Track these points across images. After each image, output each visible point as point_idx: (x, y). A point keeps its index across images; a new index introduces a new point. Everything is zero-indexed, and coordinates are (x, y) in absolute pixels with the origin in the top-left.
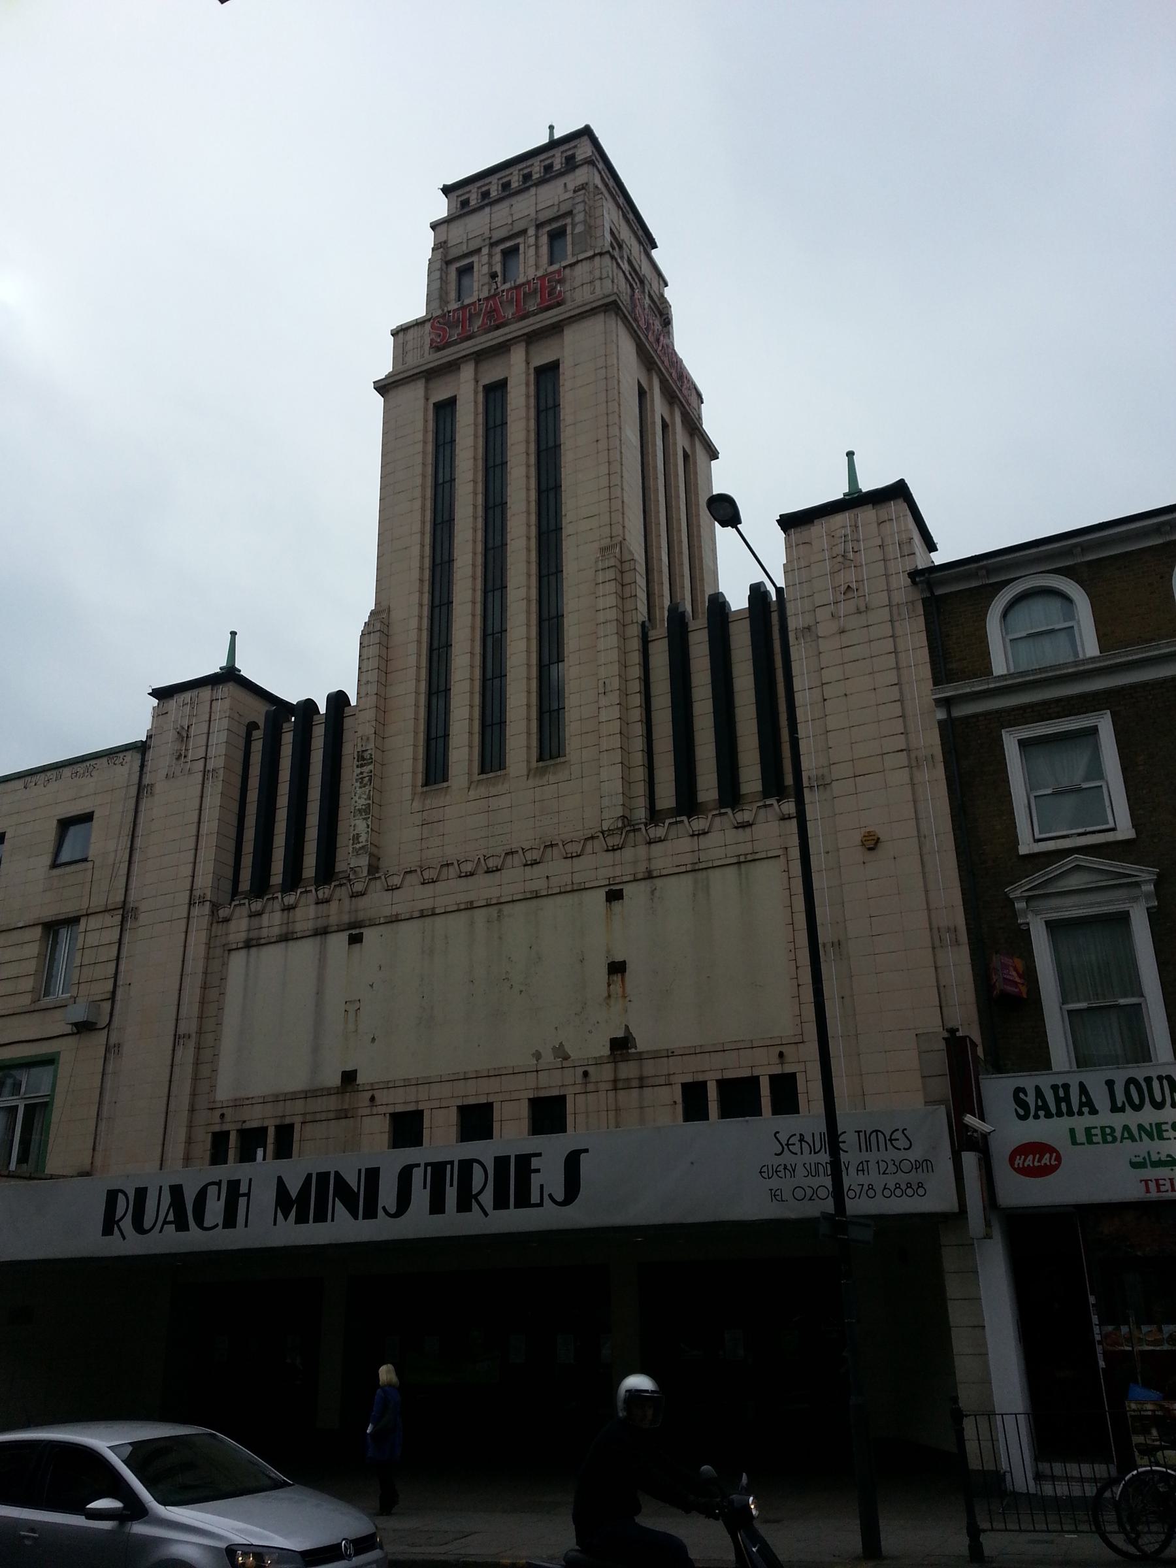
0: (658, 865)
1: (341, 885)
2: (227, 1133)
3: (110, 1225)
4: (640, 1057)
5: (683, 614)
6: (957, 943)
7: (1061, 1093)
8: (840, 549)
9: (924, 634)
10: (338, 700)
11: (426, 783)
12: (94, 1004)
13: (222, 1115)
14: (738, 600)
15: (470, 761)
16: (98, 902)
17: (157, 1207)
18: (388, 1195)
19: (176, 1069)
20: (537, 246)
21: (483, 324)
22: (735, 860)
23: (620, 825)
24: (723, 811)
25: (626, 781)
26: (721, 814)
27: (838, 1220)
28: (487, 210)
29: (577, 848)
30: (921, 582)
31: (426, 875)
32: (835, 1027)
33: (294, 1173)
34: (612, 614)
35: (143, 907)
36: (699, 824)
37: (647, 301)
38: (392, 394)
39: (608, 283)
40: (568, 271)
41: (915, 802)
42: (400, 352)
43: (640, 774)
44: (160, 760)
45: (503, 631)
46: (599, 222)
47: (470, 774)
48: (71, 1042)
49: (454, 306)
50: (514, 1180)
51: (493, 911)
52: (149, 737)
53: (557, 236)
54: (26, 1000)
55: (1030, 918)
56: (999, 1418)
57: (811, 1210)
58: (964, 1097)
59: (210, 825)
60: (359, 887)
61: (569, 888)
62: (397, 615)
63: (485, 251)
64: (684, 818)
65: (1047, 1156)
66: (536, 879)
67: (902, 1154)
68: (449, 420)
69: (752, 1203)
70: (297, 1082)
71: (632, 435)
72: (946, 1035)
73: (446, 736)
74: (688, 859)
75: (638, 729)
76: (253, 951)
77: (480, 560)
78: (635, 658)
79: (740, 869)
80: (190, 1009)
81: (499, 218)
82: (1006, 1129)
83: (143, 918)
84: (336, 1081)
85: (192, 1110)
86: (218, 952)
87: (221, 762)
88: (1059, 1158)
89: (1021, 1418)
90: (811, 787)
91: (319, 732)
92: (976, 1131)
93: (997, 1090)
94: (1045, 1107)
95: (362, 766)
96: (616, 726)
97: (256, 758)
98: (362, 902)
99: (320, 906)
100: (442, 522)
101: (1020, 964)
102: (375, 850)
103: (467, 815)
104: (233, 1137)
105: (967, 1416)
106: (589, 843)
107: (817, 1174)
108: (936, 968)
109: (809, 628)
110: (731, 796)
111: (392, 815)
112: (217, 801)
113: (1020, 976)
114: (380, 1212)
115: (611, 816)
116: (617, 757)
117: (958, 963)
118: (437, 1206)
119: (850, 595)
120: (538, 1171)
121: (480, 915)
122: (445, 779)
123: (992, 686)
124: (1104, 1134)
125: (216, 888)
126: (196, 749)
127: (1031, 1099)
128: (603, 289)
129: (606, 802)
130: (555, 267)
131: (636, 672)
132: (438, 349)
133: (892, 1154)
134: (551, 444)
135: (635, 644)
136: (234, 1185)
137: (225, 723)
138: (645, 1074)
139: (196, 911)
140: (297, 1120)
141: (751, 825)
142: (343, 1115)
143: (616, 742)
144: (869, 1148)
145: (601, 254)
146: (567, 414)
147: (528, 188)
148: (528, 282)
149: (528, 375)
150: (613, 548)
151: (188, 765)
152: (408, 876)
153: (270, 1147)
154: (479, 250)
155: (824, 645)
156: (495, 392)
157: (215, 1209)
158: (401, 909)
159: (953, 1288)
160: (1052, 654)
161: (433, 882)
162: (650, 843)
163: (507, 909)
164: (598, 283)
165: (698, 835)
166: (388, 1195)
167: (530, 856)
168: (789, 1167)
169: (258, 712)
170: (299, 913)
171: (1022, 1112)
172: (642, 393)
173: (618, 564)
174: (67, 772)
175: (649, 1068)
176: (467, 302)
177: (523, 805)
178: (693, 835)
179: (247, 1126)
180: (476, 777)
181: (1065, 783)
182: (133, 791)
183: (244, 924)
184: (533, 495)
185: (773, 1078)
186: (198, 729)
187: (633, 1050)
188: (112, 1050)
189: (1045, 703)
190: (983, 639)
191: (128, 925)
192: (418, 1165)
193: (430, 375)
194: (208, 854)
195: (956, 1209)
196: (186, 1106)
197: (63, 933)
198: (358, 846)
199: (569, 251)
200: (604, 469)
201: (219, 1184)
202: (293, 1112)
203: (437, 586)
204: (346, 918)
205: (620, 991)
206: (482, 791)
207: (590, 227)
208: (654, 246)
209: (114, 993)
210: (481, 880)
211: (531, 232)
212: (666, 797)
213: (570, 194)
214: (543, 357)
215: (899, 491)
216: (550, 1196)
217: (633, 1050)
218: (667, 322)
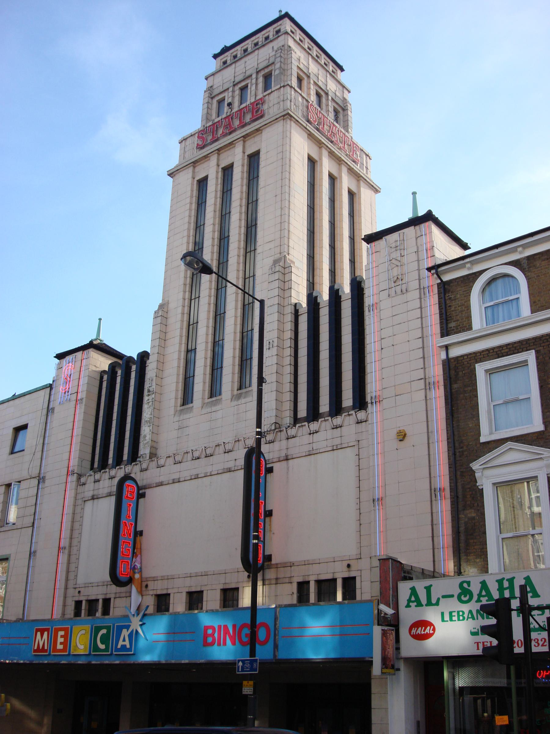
2: (81, 601)
4: (277, 566)
10: (144, 356)
13: (79, 592)
20: (257, 84)
21: (223, 132)
22: (330, 449)
23: (273, 428)
28: (256, 52)
38: (175, 178)
42: (183, 152)
46: (289, 66)
47: (203, 399)
52: (54, 381)
53: (267, 78)
60: (144, 466)
62: (172, 306)
65: (429, 628)
74: (306, 449)
76: (96, 500)
80: (66, 534)
81: (251, 63)
83: (47, 483)
85: (66, 588)
88: (434, 630)
90: (372, 403)
102: (155, 445)
104: (84, 603)
122: (220, 394)
124: (459, 616)
125: (80, 465)
138: (279, 576)
139: (70, 478)
140: (112, 596)
141: (341, 427)
145: (284, 86)
156: (228, 171)
162: (95, 482)
164: (281, 103)
165: (313, 433)
178: (310, 434)
182: (45, 412)
191: (40, 486)
193: (195, 163)
194: (76, 448)
200: (278, 213)
207: (284, 70)
209: (33, 523)
210: (203, 461)
211: (254, 76)
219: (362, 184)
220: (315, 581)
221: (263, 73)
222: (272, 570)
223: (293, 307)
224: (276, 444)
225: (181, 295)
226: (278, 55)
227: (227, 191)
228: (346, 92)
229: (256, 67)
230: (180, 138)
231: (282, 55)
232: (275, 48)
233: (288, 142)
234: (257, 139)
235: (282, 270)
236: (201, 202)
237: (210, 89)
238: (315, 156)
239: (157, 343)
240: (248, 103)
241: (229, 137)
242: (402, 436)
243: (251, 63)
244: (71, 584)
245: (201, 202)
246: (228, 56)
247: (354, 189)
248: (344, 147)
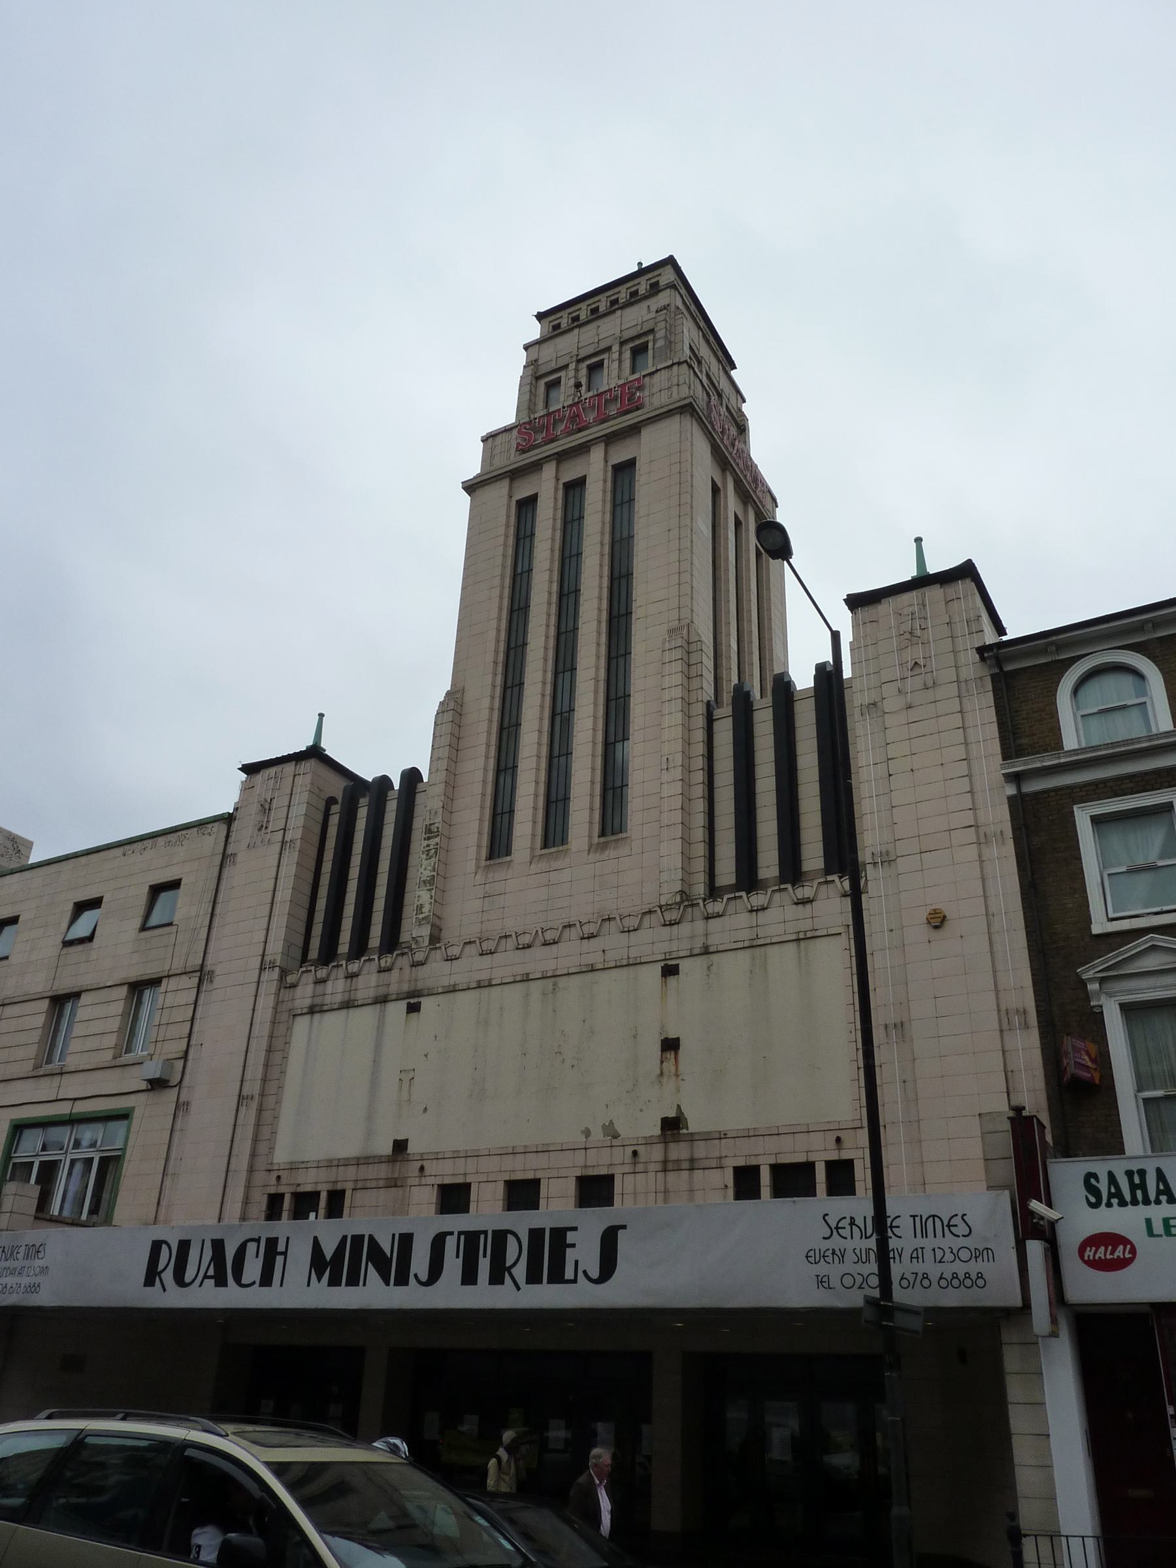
0: (715, 941)
1: (403, 954)
2: (282, 1195)
3: (152, 1276)
4: (692, 1138)
5: (748, 694)
6: (1026, 1026)
7: (1137, 1180)
8: (907, 627)
9: (993, 711)
10: (412, 777)
11: (490, 857)
12: (168, 1062)
13: (279, 1178)
14: (803, 678)
15: (533, 835)
16: (178, 966)
17: (198, 1261)
18: (420, 1263)
19: (238, 1131)
20: (620, 361)
22: (794, 937)
23: (678, 900)
24: (783, 886)
25: (687, 858)
26: (780, 890)
27: (883, 1305)
28: (576, 331)
29: (634, 922)
30: (989, 657)
31: (485, 946)
32: (887, 1094)
33: (329, 1234)
34: (678, 692)
35: (219, 970)
36: (758, 899)
37: (723, 410)
38: (479, 492)
40: (647, 379)
41: (983, 879)
43: (700, 850)
44: (244, 831)
45: (571, 710)
47: (532, 849)
48: (142, 1097)
49: (541, 412)
50: (549, 1255)
51: (550, 982)
52: (236, 809)
53: (639, 351)
54: (107, 1056)
55: (1103, 1000)
56: (1064, 1540)
57: (854, 1299)
58: (1029, 1181)
59: (285, 894)
60: (419, 956)
61: (625, 962)
63: (572, 366)
64: (743, 894)
65: (1121, 1247)
66: (592, 952)
67: (962, 1242)
68: (530, 515)
69: (796, 1289)
70: (351, 1150)
71: (704, 526)
72: (1012, 1114)
73: (511, 812)
74: (745, 935)
75: (700, 806)
76: (317, 1016)
77: (552, 643)
78: (699, 735)
79: (799, 946)
81: (586, 338)
82: (1078, 1219)
83: (218, 981)
84: (387, 1149)
85: (251, 1170)
86: (283, 1017)
87: (298, 834)
89: (1091, 1544)
91: (392, 807)
92: (1042, 1218)
93: (1067, 1175)
94: (1119, 1194)
95: (429, 838)
96: (678, 802)
97: (333, 831)
98: (422, 972)
99: (382, 974)
100: (519, 609)
101: (1093, 1049)
103: (528, 890)
104: (287, 1199)
105: (1025, 1536)
106: (647, 918)
107: (868, 1260)
108: (1004, 1052)
109: (874, 704)
110: (792, 871)
111: (457, 888)
112: (293, 869)
113: (1092, 1060)
114: (412, 1280)
115: (669, 890)
117: (1028, 1047)
118: (469, 1277)
119: (917, 671)
120: (573, 1246)
121: (535, 987)
122: (508, 853)
123: (1062, 761)
125: (286, 953)
126: (276, 823)
127: (1103, 1186)
128: (679, 395)
129: (664, 877)
130: (636, 376)
131: (699, 749)
132: (524, 452)
133: (949, 1241)
134: (625, 534)
135: (700, 722)
136: (272, 1243)
137: (305, 796)
138: (696, 1156)
139: (266, 976)
140: (349, 1187)
142: (393, 1183)
143: (677, 817)
144: (925, 1234)
145: (679, 363)
146: (641, 506)
147: (613, 312)
148: (610, 390)
149: (605, 471)
150: (682, 632)
151: (268, 836)
152: (468, 948)
153: (322, 1212)
154: (566, 367)
155: (889, 720)
156: (575, 487)
157: (253, 1268)
158: (460, 979)
159: (1015, 1390)
160: (1125, 729)
161: (492, 953)
162: (707, 918)
163: (562, 982)
165: (757, 911)
166: (420, 1263)
167: (588, 929)
168: (838, 1252)
169: (337, 787)
170: (361, 981)
171: (1093, 1200)
172: (715, 490)
173: (685, 645)
174: (161, 841)
175: (701, 1149)
176: (551, 410)
177: (583, 879)
178: (751, 911)
179: (301, 1189)
180: (539, 852)
181: (1140, 861)
183: (309, 989)
184: (606, 582)
185: (829, 1165)
186: (281, 802)
187: (684, 1131)
188: (181, 1107)
190: (1054, 715)
191: (204, 988)
192: (452, 1233)
193: (515, 475)
195: (1018, 1303)
196: (244, 1166)
197: (147, 993)
198: (421, 916)
199: (650, 361)
200: (674, 556)
201: (258, 1240)
202: (346, 1177)
203: (511, 669)
204: (405, 987)
205: (673, 1069)
206: (543, 865)
207: (670, 342)
208: (734, 367)
209: (187, 1052)
210: (538, 952)
211: (616, 348)
212: (727, 873)
213: (653, 315)
214: (620, 454)
215: (967, 571)
216: (585, 1272)
217: (684, 1131)
218: (742, 429)
220: (771, 1165)
221: (632, 345)
222: (682, 1144)
225: (489, 679)
227: (622, 503)
236: (523, 537)
244: (261, 1163)
245: (523, 537)
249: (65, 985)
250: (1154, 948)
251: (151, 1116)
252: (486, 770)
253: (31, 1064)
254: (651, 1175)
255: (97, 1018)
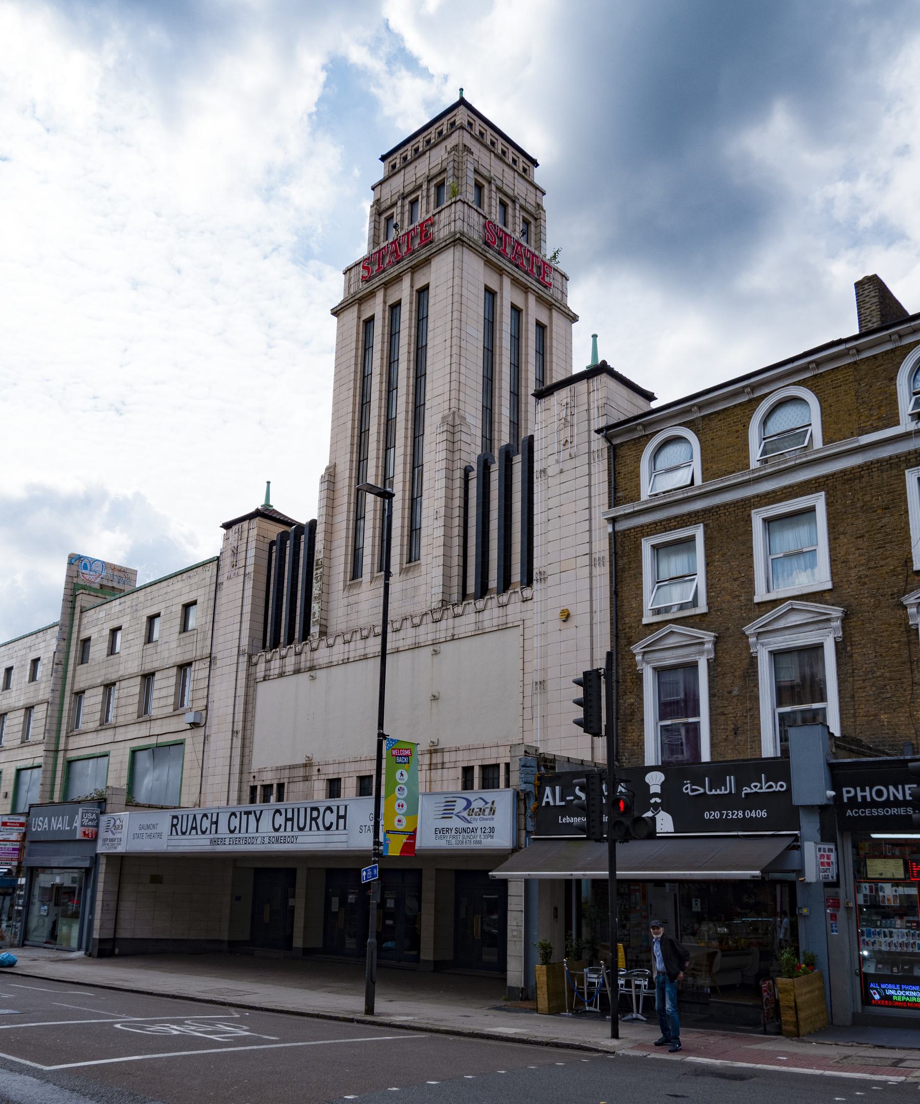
2: (472, 768)
10: (313, 524)
35: (219, 656)
38: (341, 316)
39: (459, 223)
54: (171, 709)
60: (314, 645)
62: (339, 469)
63: (425, 187)
80: (240, 717)
81: (422, 168)
96: (441, 541)
102: (323, 622)
104: (259, 788)
116: (440, 561)
125: (251, 644)
132: (367, 281)
135: (458, 483)
139: (597, 571)
140: (286, 781)
142: (306, 779)
143: (440, 551)
145: (455, 202)
164: (453, 224)
189: (669, 519)
191: (212, 667)
202: (285, 776)
219: (554, 313)
221: (435, 182)
223: (463, 471)
224: (443, 622)
226: (451, 159)
228: (539, 193)
229: (427, 173)
230: (344, 268)
231: (456, 159)
232: (448, 149)
233: (117, 596)
234: (425, 270)
235: (451, 429)
236: (366, 347)
237: (377, 202)
238: (494, 286)
239: (324, 511)
240: (417, 224)
241: (397, 267)
242: (566, 616)
243: (422, 168)
245: (366, 347)
246: (397, 159)
247: (544, 320)
248: (532, 270)
249: (148, 668)
250: (793, 609)
251: (192, 740)
252: (348, 520)
253: (135, 715)
254: (424, 772)
255: (164, 686)
